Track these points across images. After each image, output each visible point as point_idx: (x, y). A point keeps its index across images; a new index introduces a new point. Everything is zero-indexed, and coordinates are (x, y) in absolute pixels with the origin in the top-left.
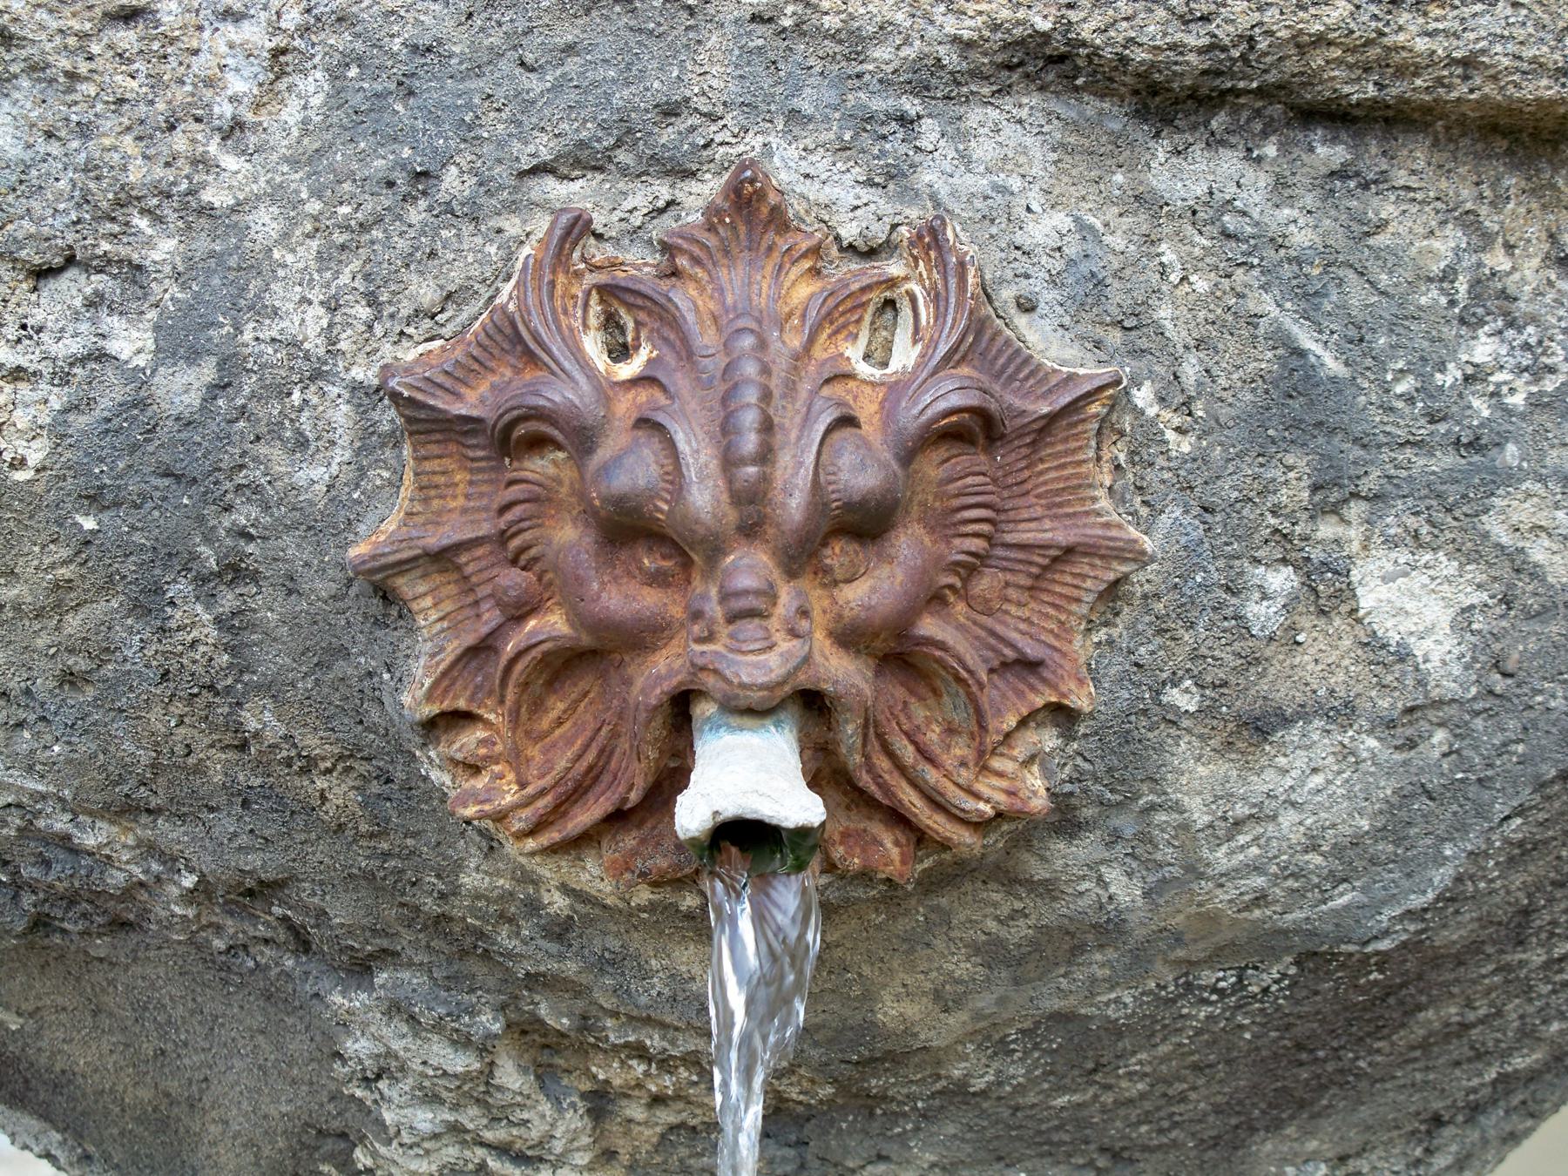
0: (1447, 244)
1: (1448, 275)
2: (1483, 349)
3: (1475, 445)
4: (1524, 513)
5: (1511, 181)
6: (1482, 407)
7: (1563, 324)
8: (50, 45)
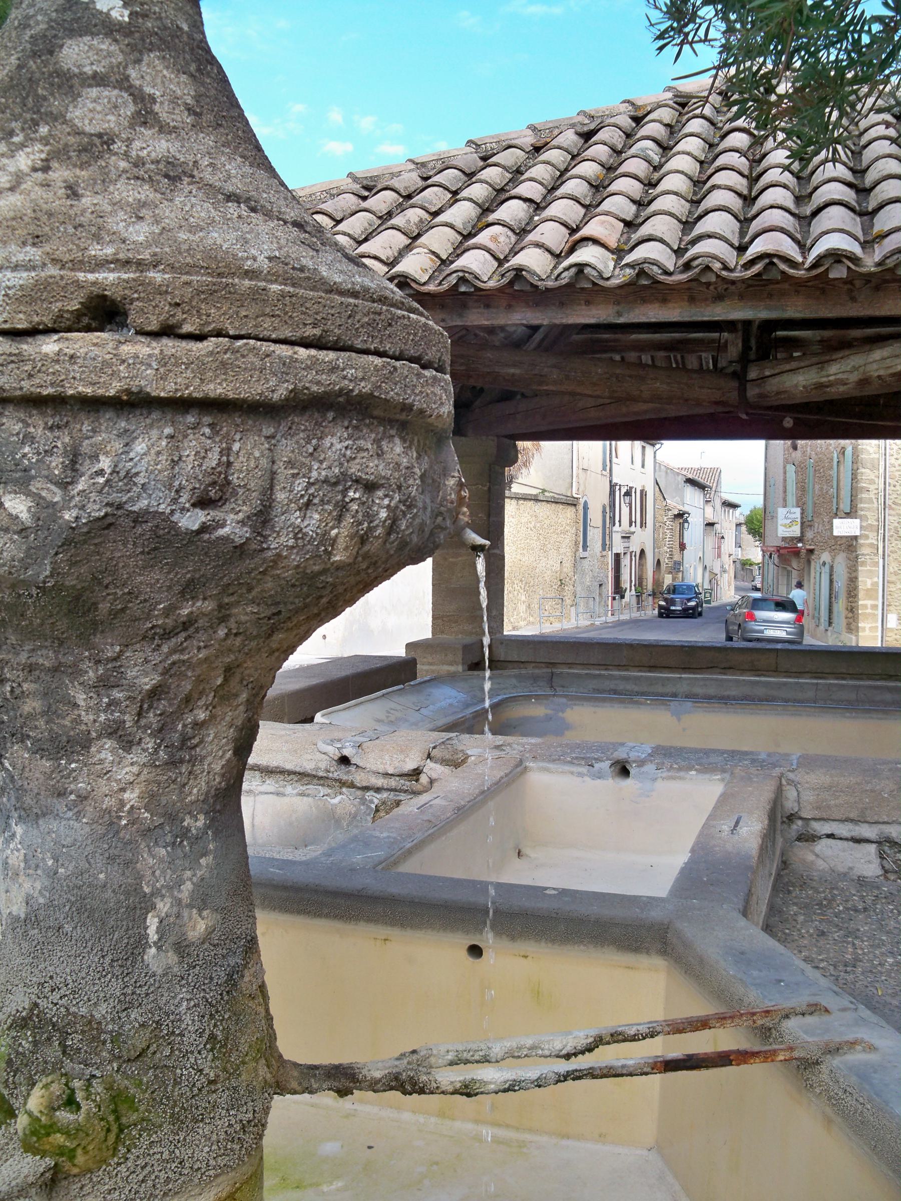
0: (18, 427)
1: (18, 434)
2: (27, 449)
3: (25, 470)
4: (39, 485)
5: (35, 412)
6: (26, 462)
7: (899, 462)
8: (295, 518)
